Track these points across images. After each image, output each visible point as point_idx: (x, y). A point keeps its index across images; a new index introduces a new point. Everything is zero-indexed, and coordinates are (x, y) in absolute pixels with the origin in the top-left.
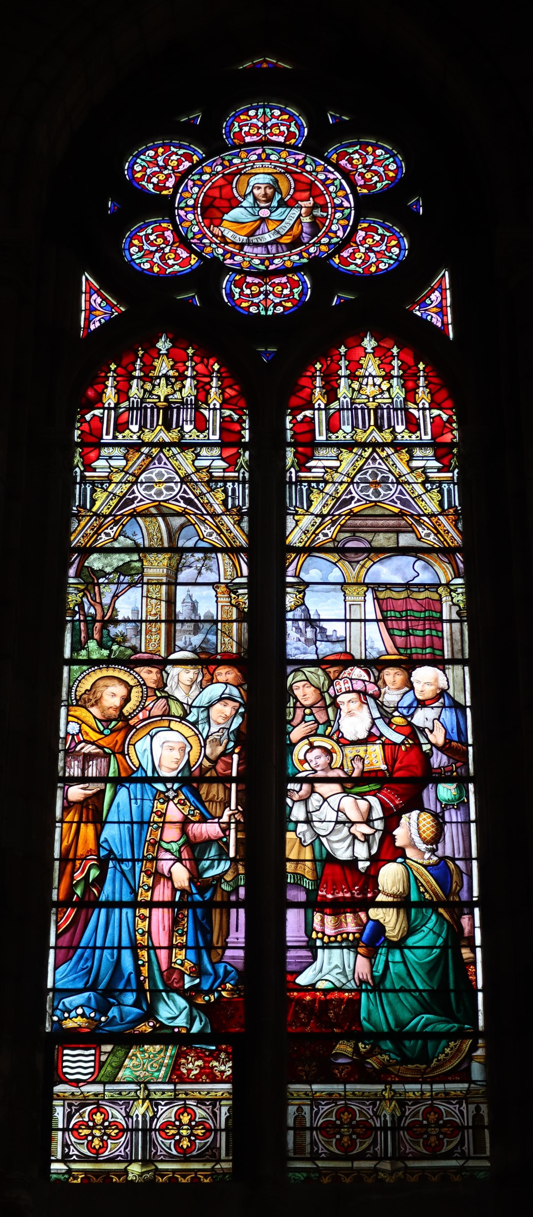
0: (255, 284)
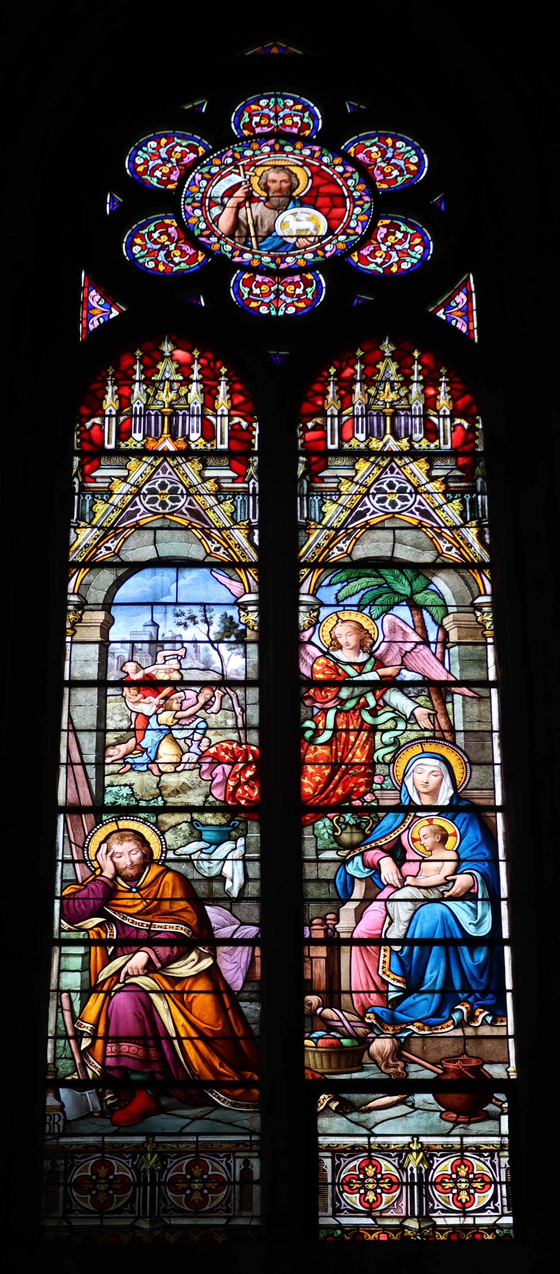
0: (265, 284)
